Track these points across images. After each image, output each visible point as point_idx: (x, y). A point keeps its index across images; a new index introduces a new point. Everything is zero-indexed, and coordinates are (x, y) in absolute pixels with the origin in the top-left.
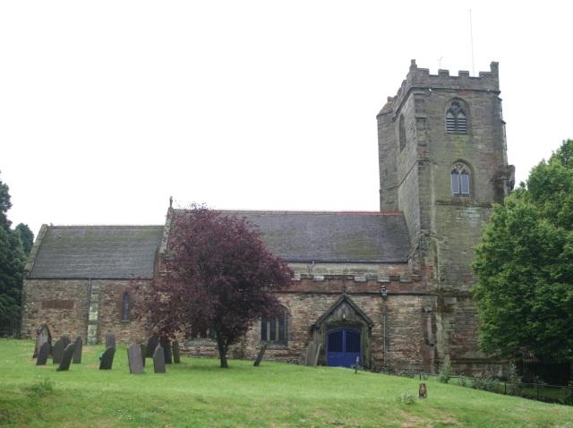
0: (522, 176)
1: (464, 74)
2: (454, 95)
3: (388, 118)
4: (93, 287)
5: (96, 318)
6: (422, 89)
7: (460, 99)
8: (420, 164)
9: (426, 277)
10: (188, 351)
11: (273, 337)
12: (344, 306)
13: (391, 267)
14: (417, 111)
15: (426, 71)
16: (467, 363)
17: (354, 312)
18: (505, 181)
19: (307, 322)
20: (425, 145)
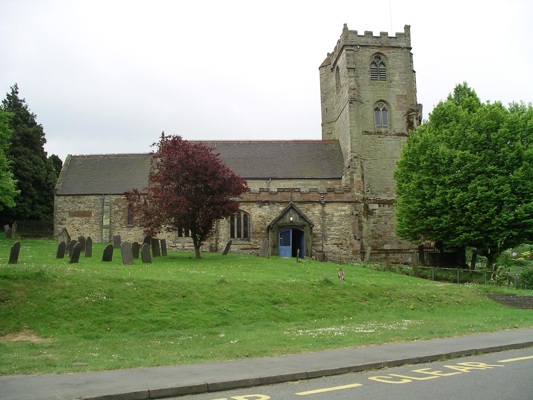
0: (426, 117)
1: (384, 34)
2: (377, 50)
3: (329, 66)
4: (105, 201)
5: (108, 223)
6: (352, 46)
7: (381, 54)
8: (350, 103)
9: (355, 189)
10: (176, 246)
11: (239, 236)
12: (291, 211)
13: (329, 182)
14: (348, 63)
15: (355, 32)
16: (386, 253)
17: (298, 216)
18: (415, 117)
19: (265, 224)
20: (354, 89)
